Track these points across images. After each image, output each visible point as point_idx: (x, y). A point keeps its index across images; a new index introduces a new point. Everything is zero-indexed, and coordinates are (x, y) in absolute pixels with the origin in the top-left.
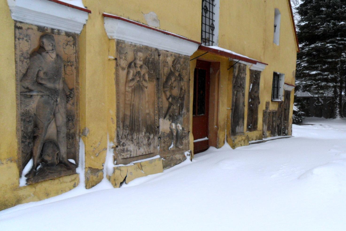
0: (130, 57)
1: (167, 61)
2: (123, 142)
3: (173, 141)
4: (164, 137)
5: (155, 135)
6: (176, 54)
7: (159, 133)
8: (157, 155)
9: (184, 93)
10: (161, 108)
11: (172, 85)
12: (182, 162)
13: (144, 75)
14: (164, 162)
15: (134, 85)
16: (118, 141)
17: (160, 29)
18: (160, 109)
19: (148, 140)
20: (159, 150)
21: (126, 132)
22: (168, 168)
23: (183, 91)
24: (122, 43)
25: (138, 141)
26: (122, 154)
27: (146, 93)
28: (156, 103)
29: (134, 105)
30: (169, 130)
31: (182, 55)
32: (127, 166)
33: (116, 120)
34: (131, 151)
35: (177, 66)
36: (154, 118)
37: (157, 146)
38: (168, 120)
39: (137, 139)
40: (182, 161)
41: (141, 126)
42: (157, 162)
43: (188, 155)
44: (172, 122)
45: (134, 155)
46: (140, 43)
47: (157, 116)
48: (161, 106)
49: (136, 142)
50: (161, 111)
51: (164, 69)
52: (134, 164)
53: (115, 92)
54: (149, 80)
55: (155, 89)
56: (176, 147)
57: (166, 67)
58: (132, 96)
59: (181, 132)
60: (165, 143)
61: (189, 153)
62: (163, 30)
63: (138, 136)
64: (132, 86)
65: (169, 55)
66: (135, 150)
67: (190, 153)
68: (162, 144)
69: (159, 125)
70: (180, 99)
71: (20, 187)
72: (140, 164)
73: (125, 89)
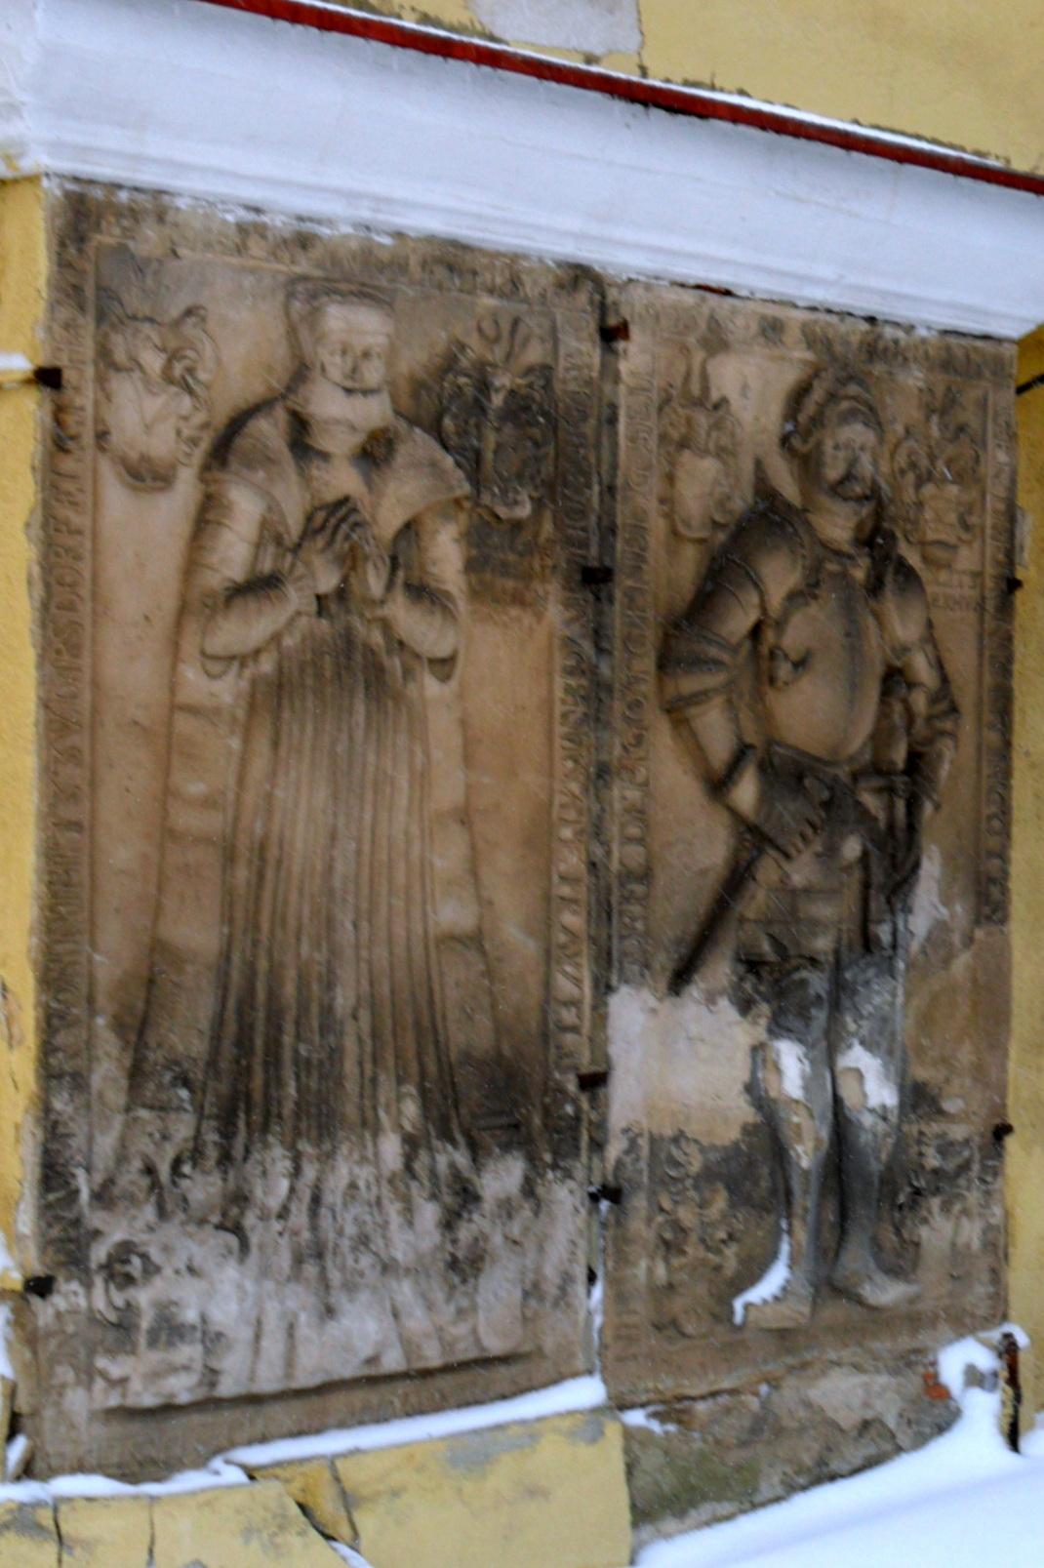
0: (240, 350)
1: (715, 396)
2: (117, 1235)
3: (790, 1232)
4: (660, 1181)
5: (555, 1167)
6: (834, 319)
7: (598, 1146)
8: (575, 1375)
9: (929, 719)
10: (627, 876)
11: (769, 636)
12: (899, 1449)
13: (410, 529)
14: (651, 1460)
15: (276, 638)
16: (55, 1232)
17: (644, 72)
18: (611, 897)
19: (449, 1223)
20: (598, 1320)
21: (165, 1137)
22: (709, 1523)
23: (920, 702)
24: (134, 213)
25: (314, 1228)
26: (101, 1362)
27: (442, 727)
28: (567, 833)
29: (273, 852)
30: (744, 1112)
31: (910, 329)
32: (153, 1499)
33: (38, 1004)
34: (213, 1340)
35: (836, 447)
36: (547, 984)
37: (580, 1288)
38: (726, 1008)
39: (293, 1207)
40: (903, 1439)
41: (350, 1067)
42: (551, 1452)
43: (974, 1378)
44: (778, 1027)
45: (252, 1379)
46: (365, 214)
47: (584, 961)
48: (622, 855)
49: (284, 1242)
50: (636, 909)
51: (670, 479)
52: (251, 1473)
53: (31, 719)
54: (475, 594)
55: (559, 682)
56: (828, 1284)
57: (704, 452)
58: (244, 761)
59: (887, 1135)
60: (683, 1253)
61: (986, 1360)
62: (686, 83)
63: (310, 1172)
64: (257, 653)
65: (740, 324)
66: (273, 1325)
67: (1000, 1356)
68: (643, 1264)
69: (607, 1059)
70: (877, 782)
71: (610, 1398)
72: (327, 1475)
73: (173, 688)
